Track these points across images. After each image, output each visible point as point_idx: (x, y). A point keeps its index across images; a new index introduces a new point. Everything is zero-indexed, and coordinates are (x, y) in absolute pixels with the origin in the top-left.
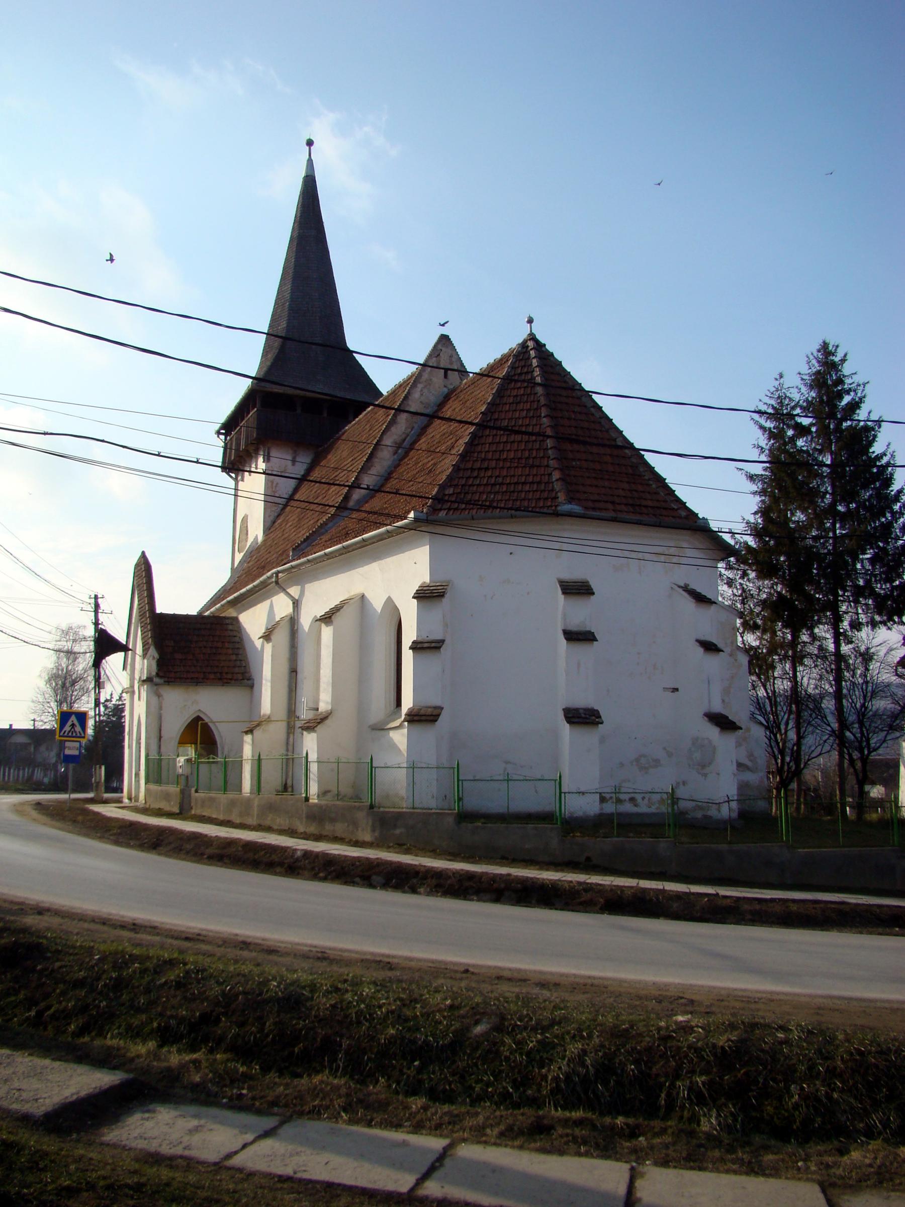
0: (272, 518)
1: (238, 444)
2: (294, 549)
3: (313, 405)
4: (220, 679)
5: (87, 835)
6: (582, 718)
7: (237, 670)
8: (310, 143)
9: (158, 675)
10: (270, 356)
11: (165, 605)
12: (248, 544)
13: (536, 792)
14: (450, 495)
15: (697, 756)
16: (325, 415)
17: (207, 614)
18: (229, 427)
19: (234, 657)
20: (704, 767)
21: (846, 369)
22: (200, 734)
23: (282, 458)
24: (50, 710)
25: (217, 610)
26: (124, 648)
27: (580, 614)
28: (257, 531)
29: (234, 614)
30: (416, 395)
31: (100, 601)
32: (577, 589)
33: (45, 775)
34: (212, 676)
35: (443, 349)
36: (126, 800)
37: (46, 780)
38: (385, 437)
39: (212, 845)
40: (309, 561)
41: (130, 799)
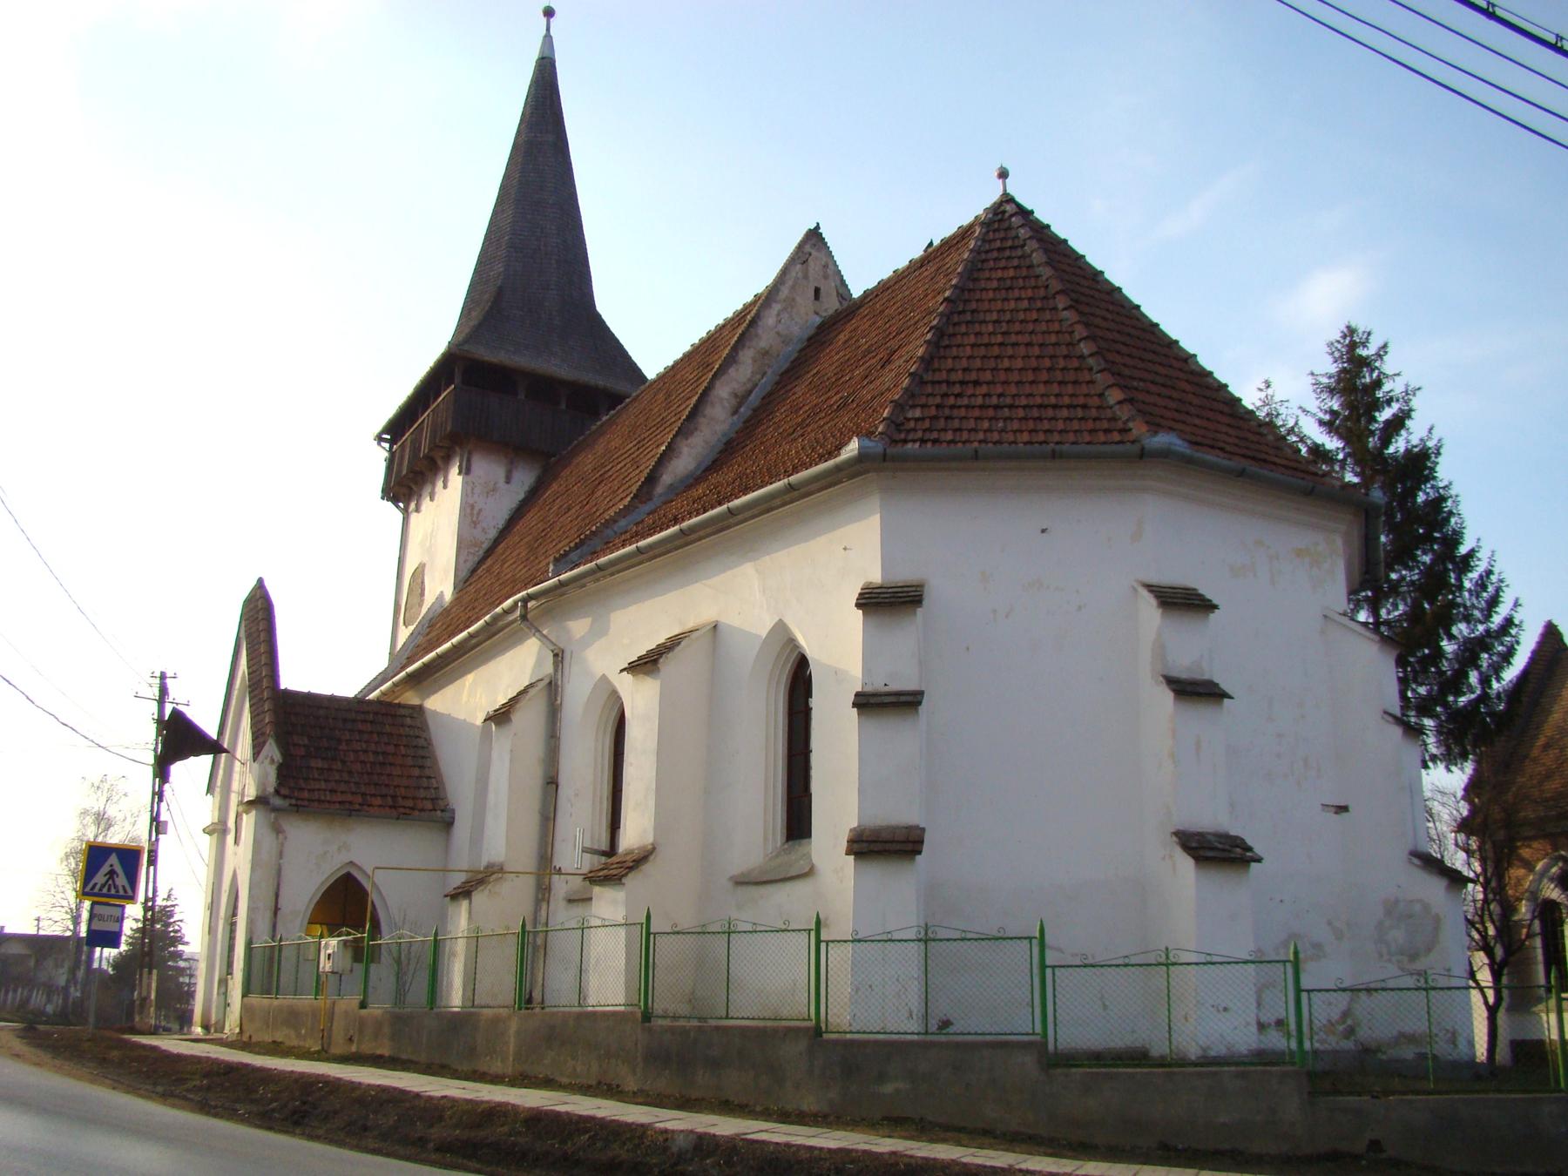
0: (470, 565)
1: (399, 471)
2: (556, 560)
3: (544, 388)
4: (393, 807)
5: (132, 1090)
6: (1218, 852)
7: (422, 794)
8: (549, 13)
9: (277, 792)
10: (474, 314)
11: (295, 676)
12: (424, 610)
13: (1105, 1007)
14: (917, 420)
15: (1397, 935)
16: (563, 406)
17: (371, 696)
18: (396, 429)
19: (416, 772)
20: (1413, 957)
21: (1388, 366)
22: (346, 903)
23: (488, 468)
24: (65, 903)
25: (384, 694)
26: (214, 748)
27: (1192, 647)
28: (441, 586)
29: (415, 701)
30: (770, 319)
31: (168, 681)
32: (1182, 602)
33: (49, 1001)
34: (378, 801)
35: (814, 253)
36: (198, 1030)
37: (50, 1009)
38: (718, 384)
39: (441, 1118)
40: (599, 568)
41: (206, 1027)
